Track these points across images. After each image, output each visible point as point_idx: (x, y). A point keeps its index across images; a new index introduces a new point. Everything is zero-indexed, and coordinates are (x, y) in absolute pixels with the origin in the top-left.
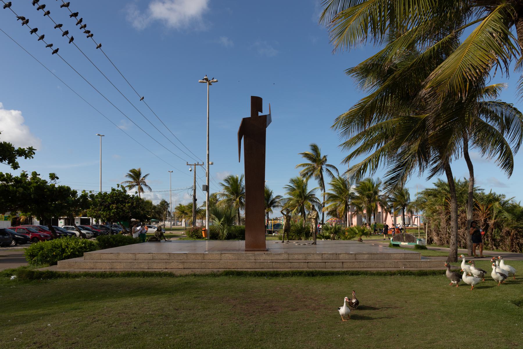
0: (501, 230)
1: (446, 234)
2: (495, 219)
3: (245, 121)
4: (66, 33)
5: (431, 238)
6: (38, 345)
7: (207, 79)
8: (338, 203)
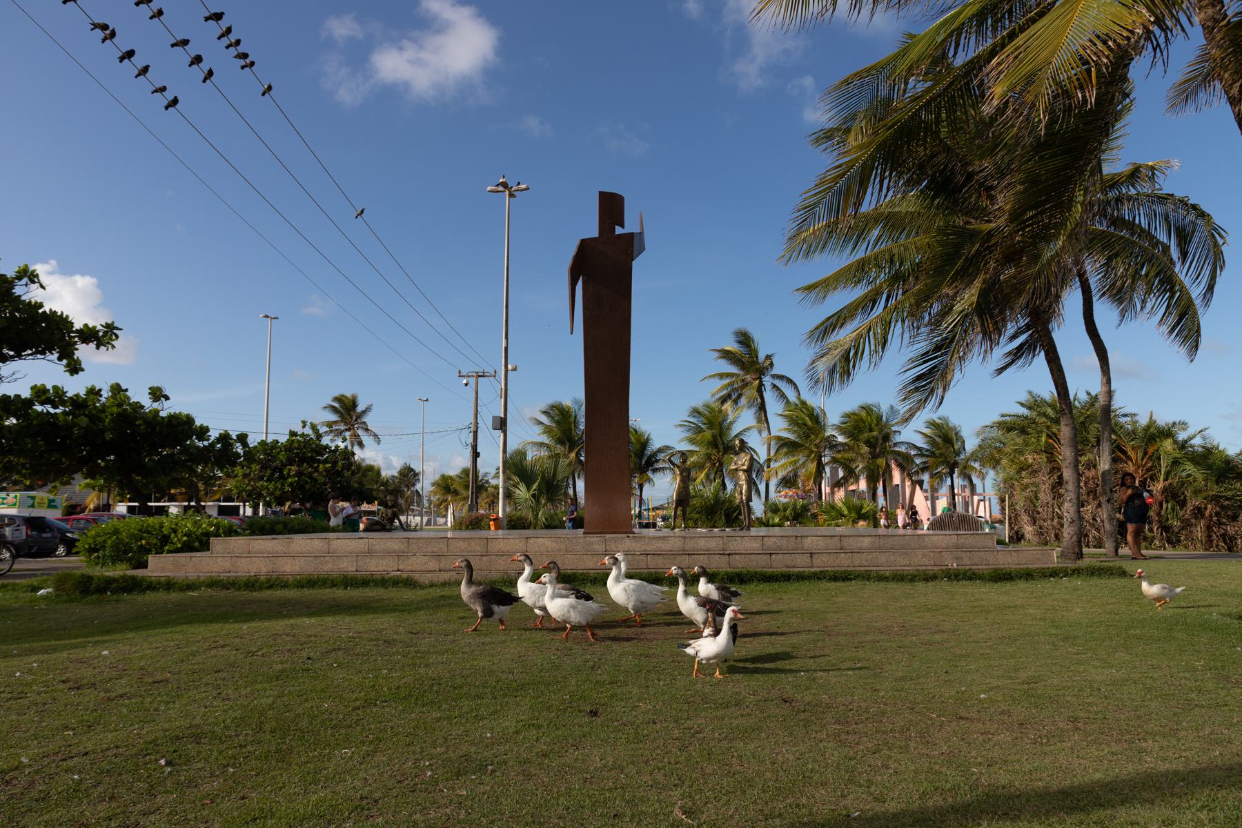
0: (1183, 504)
1: (1052, 520)
2: (1166, 480)
3: (585, 246)
4: (197, 60)
5: (1017, 533)
6: (71, 684)
7: (505, 185)
8: (801, 458)
